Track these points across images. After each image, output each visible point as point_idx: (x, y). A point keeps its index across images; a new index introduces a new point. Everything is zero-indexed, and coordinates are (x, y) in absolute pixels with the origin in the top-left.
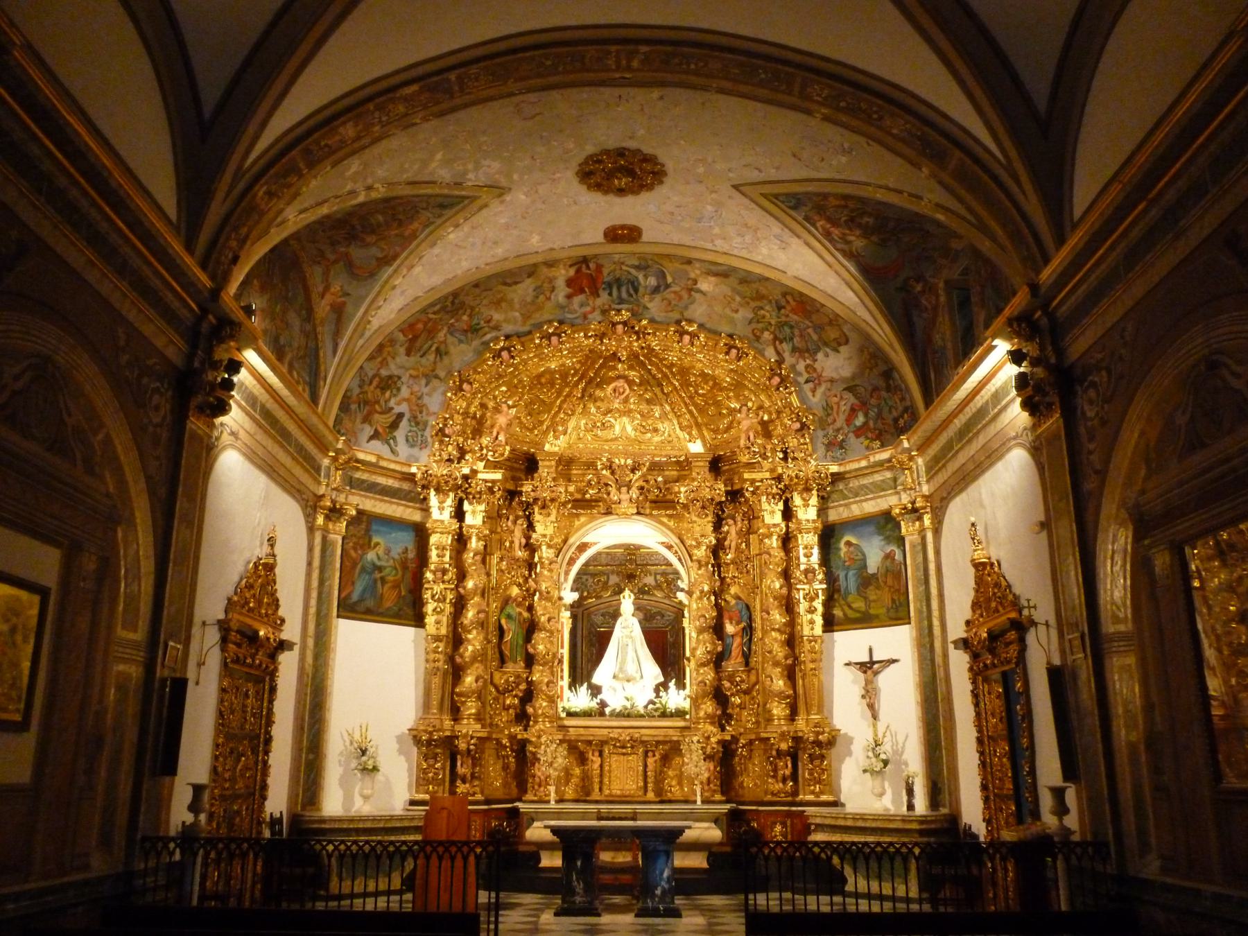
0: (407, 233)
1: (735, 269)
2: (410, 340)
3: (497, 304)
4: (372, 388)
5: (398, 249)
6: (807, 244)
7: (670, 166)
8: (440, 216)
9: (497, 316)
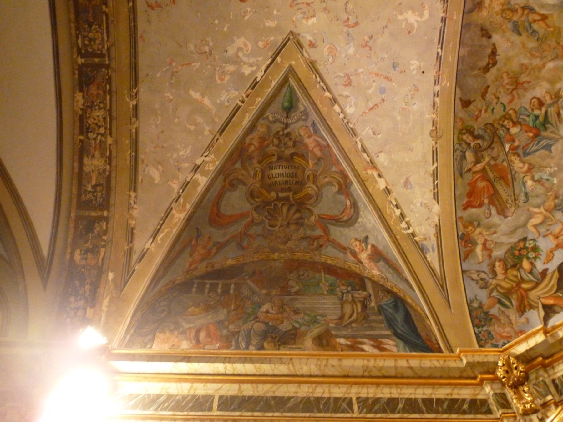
0: (318, 153)
2: (491, 203)
3: (517, 84)
4: (500, 276)
8: (305, 113)
9: (540, 91)
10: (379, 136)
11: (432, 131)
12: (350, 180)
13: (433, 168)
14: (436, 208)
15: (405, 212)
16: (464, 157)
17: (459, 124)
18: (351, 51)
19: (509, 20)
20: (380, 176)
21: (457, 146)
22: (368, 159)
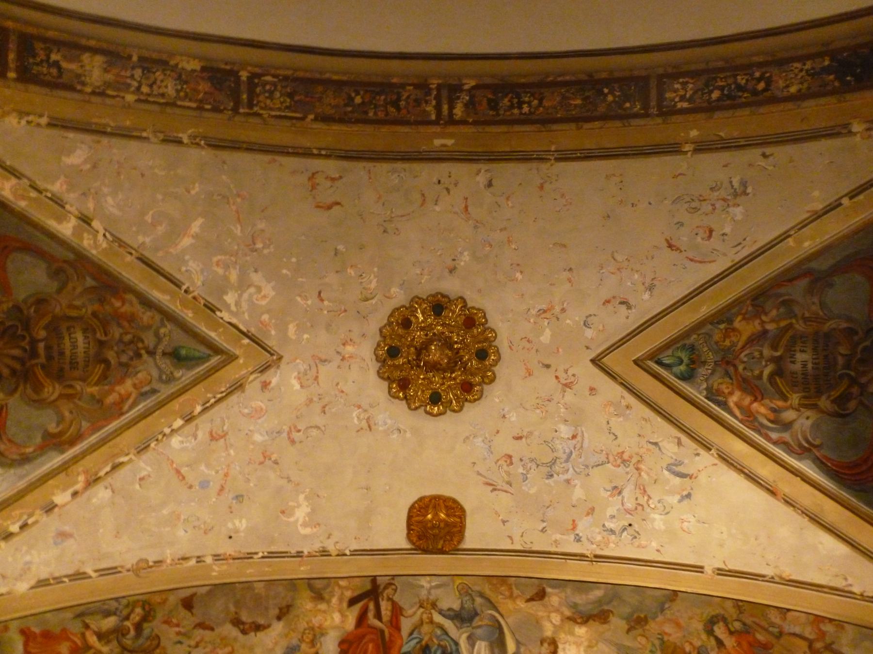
0: (111, 399)
1: (615, 591)
5: (85, 425)
6: (725, 459)
7: (505, 329)
10: (137, 487)
11: (147, 561)
12: (67, 450)
13: (89, 571)
14: (22, 587)
15: (15, 540)
16: (107, 614)
17: (157, 599)
18: (258, 438)
19: (301, 640)
20: (75, 494)
21: (124, 601)
22: (102, 473)
